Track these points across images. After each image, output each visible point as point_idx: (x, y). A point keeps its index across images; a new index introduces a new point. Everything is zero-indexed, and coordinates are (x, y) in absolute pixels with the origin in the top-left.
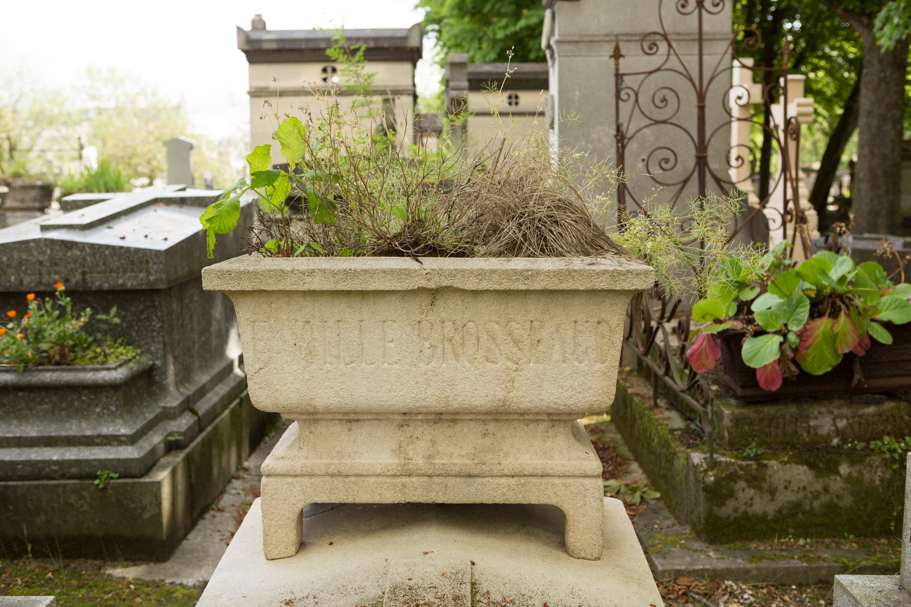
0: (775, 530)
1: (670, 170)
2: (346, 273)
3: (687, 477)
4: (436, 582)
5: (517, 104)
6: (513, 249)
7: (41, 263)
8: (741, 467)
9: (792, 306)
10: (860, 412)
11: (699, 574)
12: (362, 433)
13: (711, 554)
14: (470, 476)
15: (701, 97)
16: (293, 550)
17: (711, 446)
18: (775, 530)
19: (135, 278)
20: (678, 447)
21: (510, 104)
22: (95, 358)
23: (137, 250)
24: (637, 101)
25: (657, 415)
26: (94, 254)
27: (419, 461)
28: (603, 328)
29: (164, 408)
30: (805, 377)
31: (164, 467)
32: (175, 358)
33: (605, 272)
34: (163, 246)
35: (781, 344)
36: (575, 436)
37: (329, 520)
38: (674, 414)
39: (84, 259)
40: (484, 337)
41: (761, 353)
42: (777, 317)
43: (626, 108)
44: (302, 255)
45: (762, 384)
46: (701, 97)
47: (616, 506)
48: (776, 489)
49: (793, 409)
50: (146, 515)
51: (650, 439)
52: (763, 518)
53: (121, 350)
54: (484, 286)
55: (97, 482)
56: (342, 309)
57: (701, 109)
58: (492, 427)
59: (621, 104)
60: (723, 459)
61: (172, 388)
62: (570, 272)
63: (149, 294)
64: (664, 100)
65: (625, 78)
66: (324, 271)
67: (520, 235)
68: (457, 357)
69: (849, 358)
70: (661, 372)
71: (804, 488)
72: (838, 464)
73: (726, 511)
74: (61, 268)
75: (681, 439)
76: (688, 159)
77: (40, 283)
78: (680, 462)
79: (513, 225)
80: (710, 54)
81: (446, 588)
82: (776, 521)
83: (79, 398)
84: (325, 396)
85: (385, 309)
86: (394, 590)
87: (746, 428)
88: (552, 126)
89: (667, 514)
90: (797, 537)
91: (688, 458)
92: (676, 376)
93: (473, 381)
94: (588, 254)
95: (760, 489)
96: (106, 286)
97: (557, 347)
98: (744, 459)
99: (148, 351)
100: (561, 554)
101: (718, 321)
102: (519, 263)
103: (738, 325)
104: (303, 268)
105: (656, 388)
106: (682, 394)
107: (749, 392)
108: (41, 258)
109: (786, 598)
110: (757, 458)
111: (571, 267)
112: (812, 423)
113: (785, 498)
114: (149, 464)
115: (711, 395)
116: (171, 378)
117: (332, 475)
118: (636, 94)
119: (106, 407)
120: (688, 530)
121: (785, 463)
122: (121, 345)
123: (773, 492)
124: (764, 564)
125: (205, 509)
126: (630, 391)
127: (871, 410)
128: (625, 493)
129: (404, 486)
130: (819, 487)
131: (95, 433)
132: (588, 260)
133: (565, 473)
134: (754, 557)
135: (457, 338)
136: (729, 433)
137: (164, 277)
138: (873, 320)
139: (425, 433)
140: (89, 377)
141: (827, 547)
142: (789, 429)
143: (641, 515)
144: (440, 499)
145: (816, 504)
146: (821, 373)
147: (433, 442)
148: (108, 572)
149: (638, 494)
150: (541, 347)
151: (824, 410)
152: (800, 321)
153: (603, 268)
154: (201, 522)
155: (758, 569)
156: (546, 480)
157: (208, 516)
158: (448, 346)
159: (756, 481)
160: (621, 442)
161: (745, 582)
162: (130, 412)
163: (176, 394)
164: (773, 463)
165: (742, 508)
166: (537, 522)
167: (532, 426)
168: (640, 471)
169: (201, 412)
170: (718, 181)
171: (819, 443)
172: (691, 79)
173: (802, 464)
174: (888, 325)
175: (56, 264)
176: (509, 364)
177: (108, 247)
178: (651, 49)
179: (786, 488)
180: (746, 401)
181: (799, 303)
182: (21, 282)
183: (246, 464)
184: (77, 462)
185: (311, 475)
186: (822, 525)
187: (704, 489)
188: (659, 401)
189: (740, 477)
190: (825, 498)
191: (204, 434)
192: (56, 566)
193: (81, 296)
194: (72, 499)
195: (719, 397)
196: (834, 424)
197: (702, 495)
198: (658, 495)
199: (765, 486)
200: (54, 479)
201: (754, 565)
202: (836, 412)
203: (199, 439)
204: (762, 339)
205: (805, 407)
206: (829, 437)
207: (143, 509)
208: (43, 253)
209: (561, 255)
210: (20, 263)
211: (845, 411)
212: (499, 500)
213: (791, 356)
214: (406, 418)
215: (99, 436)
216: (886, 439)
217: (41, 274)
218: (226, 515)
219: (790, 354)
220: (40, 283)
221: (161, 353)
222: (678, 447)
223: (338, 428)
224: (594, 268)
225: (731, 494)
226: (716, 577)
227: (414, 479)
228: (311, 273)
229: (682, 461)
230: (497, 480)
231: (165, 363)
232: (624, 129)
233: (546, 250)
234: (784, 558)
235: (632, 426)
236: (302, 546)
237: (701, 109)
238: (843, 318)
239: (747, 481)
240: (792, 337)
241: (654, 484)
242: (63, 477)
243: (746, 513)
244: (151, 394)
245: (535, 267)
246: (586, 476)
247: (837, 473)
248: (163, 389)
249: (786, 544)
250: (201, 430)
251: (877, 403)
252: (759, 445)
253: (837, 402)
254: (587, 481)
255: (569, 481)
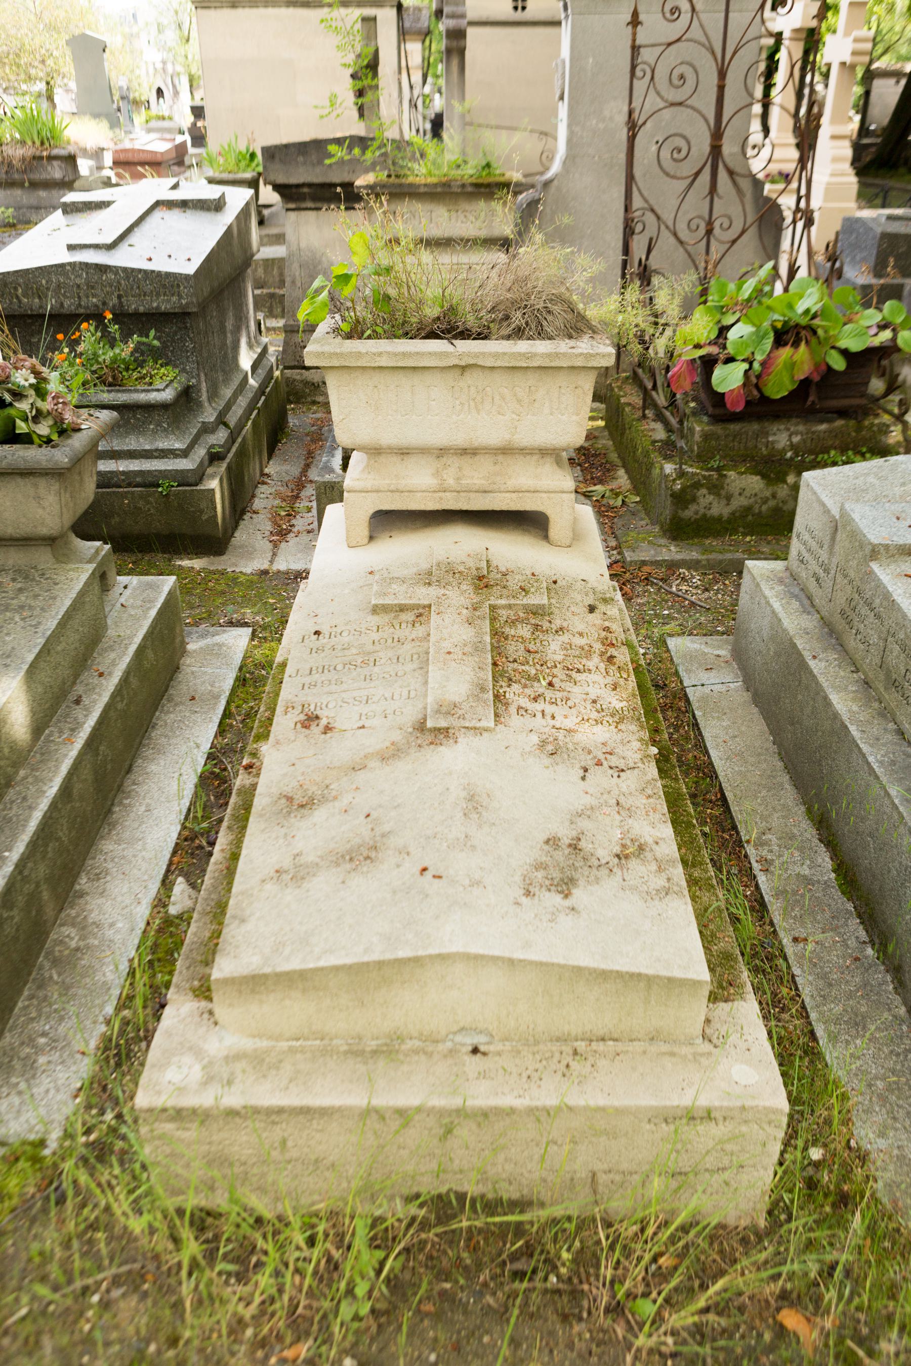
0: (727, 529)
1: (689, 143)
2: (404, 354)
3: (660, 485)
4: (464, 560)
5: (524, 8)
6: (518, 333)
7: (78, 286)
8: (704, 477)
9: (759, 337)
10: (814, 429)
11: (657, 564)
12: (411, 462)
13: (672, 548)
14: (485, 492)
15: (722, 75)
16: (366, 540)
17: (681, 459)
18: (727, 529)
19: (168, 301)
20: (656, 457)
21: (516, 8)
22: (141, 378)
23: (168, 274)
24: (652, 78)
25: (644, 426)
26: (128, 278)
27: (451, 482)
28: (579, 391)
29: (203, 423)
30: (764, 399)
31: (212, 477)
32: (206, 375)
33: (581, 354)
34: (190, 269)
35: (746, 372)
36: (557, 464)
37: (387, 521)
38: (659, 426)
39: (119, 282)
40: (497, 397)
41: (728, 379)
42: (747, 346)
43: (640, 86)
44: (369, 337)
45: (728, 405)
46: (722, 75)
47: (587, 512)
48: (732, 496)
49: (755, 426)
50: (205, 517)
51: (635, 448)
52: (719, 519)
53: (163, 370)
54: (498, 364)
55: (160, 489)
56: (400, 377)
57: (721, 88)
58: (500, 458)
59: (635, 81)
60: (690, 470)
61: (206, 404)
62: (557, 355)
63: (181, 317)
64: (682, 77)
65: (642, 50)
66: (388, 353)
67: (523, 322)
68: (478, 411)
69: (805, 384)
70: (649, 386)
71: (756, 495)
72: (786, 474)
73: (689, 513)
74: (98, 292)
75: (660, 451)
76: (702, 145)
77: (80, 305)
78: (656, 471)
79: (519, 314)
80: (741, 11)
81: (471, 564)
82: (729, 521)
83: (134, 416)
84: (388, 437)
85: (428, 377)
86: (438, 565)
87: (713, 442)
88: (562, 98)
89: (643, 516)
90: (745, 535)
91: (662, 468)
92: (660, 391)
93: (489, 429)
94: (570, 337)
95: (718, 495)
96: (141, 309)
97: (547, 405)
98: (708, 470)
99: (183, 370)
100: (544, 543)
101: (698, 346)
102: (522, 346)
103: (714, 350)
104: (374, 350)
105: (645, 400)
106: (664, 411)
107: (718, 411)
108: (78, 281)
109: (727, 582)
110: (719, 469)
111: (558, 350)
112: (770, 439)
113: (738, 502)
114: (199, 475)
115: (688, 411)
116: (204, 397)
117: (392, 491)
118: (653, 71)
119: (159, 424)
120: (657, 529)
121: (742, 473)
122: (162, 366)
123: (729, 498)
124: (713, 556)
125: (243, 512)
126: (623, 400)
127: (823, 427)
128: (609, 498)
129: (441, 499)
130: (768, 494)
131: (153, 448)
132: (572, 343)
133: (552, 489)
134: (706, 551)
135: (479, 398)
136: (699, 447)
137: (195, 300)
138: (833, 347)
139: (454, 462)
140: (142, 397)
141: (769, 543)
142: (750, 444)
143: (621, 516)
144: (465, 507)
145: (764, 508)
146: (778, 397)
147: (460, 468)
148: (179, 563)
149: (620, 498)
150: (536, 405)
151: (782, 427)
152: (764, 352)
153: (580, 351)
154: (242, 523)
155: (708, 560)
156: (536, 494)
157: (245, 517)
158: (472, 403)
159: (716, 488)
160: (612, 448)
161: (696, 570)
162: (178, 428)
163: (210, 410)
164: (732, 474)
165: (702, 511)
166: (530, 522)
167: (528, 457)
168: (626, 477)
169: (232, 424)
170: (731, 173)
171: (774, 456)
172: (713, 53)
173: (756, 474)
174: (845, 353)
175: (93, 287)
176: (514, 416)
177: (140, 271)
178: (673, 13)
179: (740, 494)
180: (717, 419)
181: (766, 334)
182: (62, 305)
183: (266, 471)
184: (141, 473)
185: (378, 491)
186: (766, 525)
187: (671, 495)
188: (647, 412)
189: (702, 486)
190: (772, 503)
191: (236, 445)
192: (134, 559)
193: (132, 322)
194: (141, 504)
195: (694, 413)
196: (790, 439)
197: (670, 499)
198: (638, 499)
199: (723, 493)
200: (120, 487)
201: (704, 557)
202: (792, 429)
203: (234, 449)
204: (731, 365)
205: (766, 424)
206: (784, 451)
207: (202, 512)
208: (80, 276)
209: (550, 338)
210: (59, 286)
211: (801, 428)
212: (505, 508)
213: (753, 382)
214: (442, 452)
215: (156, 450)
216: (833, 453)
217: (79, 297)
218: (261, 516)
219: (754, 380)
220: (80, 305)
221: (195, 372)
222: (656, 457)
223: (395, 459)
224: (574, 351)
225: (694, 499)
226: (672, 566)
227: (448, 494)
228: (380, 354)
229: (657, 471)
230: (504, 495)
231: (199, 382)
232: (636, 115)
233: (541, 334)
234: (730, 551)
235: (622, 434)
236: (371, 538)
237: (721, 88)
238: (803, 346)
239: (708, 489)
240: (756, 366)
241: (636, 490)
242: (129, 485)
243: (705, 515)
244: (190, 410)
245: (533, 350)
246: (563, 492)
247: (785, 482)
248: (200, 405)
249: (735, 540)
250: (234, 442)
251: (829, 421)
252: (723, 458)
253: (794, 420)
254: (564, 495)
255: (552, 495)
